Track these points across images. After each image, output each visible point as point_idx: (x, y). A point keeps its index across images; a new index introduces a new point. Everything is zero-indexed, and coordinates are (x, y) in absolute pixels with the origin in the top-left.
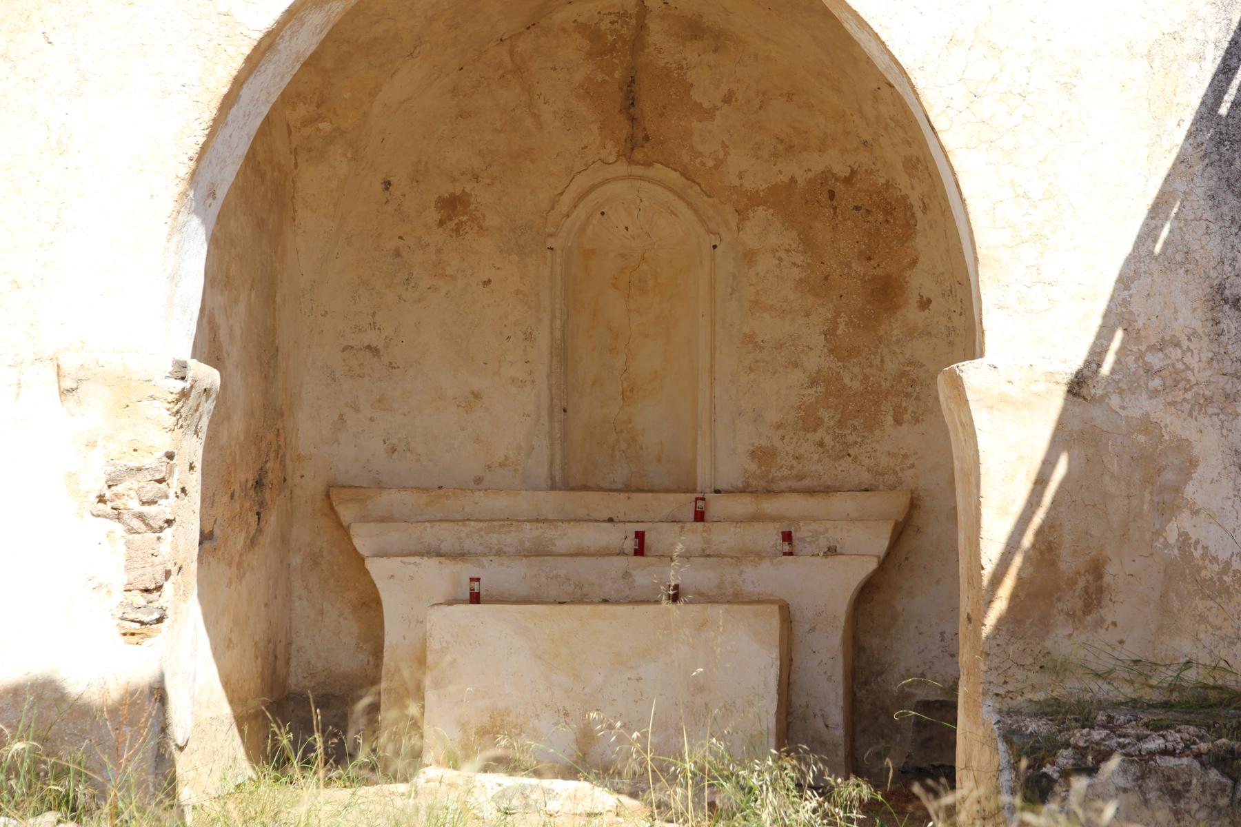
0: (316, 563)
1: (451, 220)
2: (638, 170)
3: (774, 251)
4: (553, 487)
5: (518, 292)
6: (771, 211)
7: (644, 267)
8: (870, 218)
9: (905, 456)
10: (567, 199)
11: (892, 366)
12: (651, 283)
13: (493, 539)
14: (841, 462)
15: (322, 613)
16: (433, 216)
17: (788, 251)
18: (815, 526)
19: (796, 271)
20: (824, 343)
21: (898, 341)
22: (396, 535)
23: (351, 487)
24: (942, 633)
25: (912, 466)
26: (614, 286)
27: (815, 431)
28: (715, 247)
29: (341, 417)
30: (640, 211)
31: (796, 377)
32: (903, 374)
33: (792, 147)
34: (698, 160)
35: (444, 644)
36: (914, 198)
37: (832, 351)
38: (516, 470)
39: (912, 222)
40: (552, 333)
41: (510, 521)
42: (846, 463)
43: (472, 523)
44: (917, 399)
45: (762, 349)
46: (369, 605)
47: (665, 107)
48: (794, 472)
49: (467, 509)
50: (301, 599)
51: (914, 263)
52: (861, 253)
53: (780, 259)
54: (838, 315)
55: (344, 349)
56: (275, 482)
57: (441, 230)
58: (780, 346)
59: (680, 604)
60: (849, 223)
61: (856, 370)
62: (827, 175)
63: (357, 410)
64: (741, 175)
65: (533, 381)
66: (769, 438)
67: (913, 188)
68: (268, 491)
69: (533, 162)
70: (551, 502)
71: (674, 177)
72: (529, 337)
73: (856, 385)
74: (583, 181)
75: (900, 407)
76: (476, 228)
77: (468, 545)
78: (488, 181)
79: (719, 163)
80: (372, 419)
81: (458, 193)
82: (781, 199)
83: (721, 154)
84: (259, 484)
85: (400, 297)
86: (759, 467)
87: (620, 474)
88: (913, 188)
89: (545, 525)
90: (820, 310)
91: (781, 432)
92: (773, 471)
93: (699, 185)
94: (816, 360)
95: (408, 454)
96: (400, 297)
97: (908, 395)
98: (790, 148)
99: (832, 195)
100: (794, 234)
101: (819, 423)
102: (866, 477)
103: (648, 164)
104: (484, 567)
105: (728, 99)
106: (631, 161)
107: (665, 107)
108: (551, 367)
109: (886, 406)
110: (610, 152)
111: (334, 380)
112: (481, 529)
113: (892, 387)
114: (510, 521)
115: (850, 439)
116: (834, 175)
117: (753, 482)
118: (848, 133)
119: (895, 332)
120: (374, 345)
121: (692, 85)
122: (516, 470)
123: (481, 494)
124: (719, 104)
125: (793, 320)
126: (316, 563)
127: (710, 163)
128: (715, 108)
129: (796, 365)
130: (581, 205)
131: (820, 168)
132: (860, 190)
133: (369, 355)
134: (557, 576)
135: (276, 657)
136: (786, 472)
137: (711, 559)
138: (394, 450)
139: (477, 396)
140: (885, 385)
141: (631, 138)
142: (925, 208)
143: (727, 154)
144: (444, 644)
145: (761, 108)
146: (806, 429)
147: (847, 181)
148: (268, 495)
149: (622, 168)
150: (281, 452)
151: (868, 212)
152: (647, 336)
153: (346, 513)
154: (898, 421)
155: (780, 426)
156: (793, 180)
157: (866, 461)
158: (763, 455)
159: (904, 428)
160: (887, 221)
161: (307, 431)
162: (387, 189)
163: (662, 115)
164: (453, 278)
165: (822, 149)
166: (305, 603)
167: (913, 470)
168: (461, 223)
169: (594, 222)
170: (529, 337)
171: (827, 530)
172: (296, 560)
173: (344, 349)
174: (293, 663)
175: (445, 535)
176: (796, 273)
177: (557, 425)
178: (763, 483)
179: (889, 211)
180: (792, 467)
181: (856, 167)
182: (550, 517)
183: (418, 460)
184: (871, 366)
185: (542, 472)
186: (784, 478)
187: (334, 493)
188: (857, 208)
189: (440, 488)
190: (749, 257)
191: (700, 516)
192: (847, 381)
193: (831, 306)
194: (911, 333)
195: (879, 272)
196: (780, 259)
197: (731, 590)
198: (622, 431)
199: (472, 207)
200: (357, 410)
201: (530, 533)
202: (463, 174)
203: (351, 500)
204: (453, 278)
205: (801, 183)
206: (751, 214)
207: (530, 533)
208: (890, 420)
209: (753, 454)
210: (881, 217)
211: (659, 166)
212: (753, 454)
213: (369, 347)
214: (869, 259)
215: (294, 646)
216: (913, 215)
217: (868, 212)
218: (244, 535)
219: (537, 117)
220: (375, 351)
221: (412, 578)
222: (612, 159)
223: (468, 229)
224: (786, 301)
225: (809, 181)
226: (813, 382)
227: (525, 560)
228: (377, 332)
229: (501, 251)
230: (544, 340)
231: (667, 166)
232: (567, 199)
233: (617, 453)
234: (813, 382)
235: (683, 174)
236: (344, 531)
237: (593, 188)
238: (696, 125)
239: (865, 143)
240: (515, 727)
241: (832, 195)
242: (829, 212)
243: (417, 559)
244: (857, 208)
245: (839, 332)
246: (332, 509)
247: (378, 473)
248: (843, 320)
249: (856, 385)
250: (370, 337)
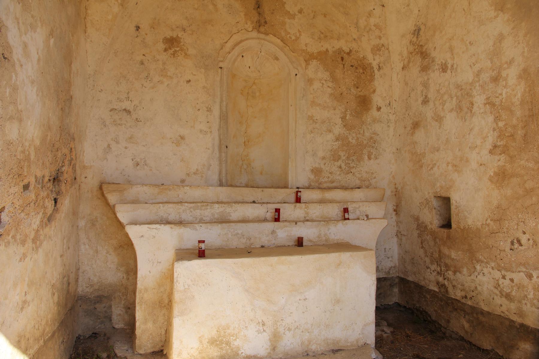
0: (93, 225)
1: (171, 49)
2: (262, 36)
3: (320, 80)
4: (221, 185)
5: (204, 87)
6: (319, 62)
7: (254, 87)
8: (357, 71)
9: (372, 173)
10: (229, 45)
11: (367, 134)
12: (257, 94)
13: (198, 213)
14: (348, 175)
15: (97, 252)
16: (161, 46)
17: (326, 81)
18: (354, 205)
19: (329, 90)
20: (341, 122)
21: (370, 123)
22: (142, 212)
23: (113, 183)
24: (385, 249)
25: (375, 178)
26: (242, 94)
27: (338, 161)
28: (296, 75)
29: (109, 146)
30: (259, 57)
31: (330, 136)
32: (371, 138)
33: (327, 36)
34: (288, 36)
35: (186, 287)
36: (375, 64)
37: (345, 126)
38: (202, 176)
39: (373, 74)
40: (221, 109)
41: (205, 203)
42: (350, 176)
43: (186, 204)
44: (376, 149)
45: (316, 123)
46: (127, 248)
47: (274, 10)
48: (330, 179)
49: (180, 196)
50: (84, 244)
51: (374, 91)
52: (354, 85)
53: (323, 84)
54: (346, 111)
55: (111, 110)
56: (69, 179)
57: (165, 53)
58: (323, 122)
60: (349, 72)
61: (354, 135)
62: (340, 51)
63: (118, 143)
64: (306, 45)
65: (211, 132)
66: (319, 164)
67: (374, 60)
68: (64, 184)
69: (213, 25)
70: (224, 193)
71: (279, 41)
72: (209, 110)
73: (354, 141)
74: (236, 38)
75: (370, 152)
76: (183, 54)
77: (184, 217)
78: (190, 32)
79: (297, 39)
80: (126, 148)
81: (175, 36)
82: (322, 57)
83: (298, 34)
84: (56, 180)
85: (142, 85)
86: (315, 177)
87: (244, 179)
88: (374, 60)
89: (226, 205)
90: (340, 108)
91: (324, 161)
92: (321, 178)
94: (338, 130)
95: (146, 167)
96: (142, 85)
97: (373, 147)
98: (326, 37)
99: (342, 59)
100: (328, 74)
101: (339, 158)
102: (358, 182)
103: (267, 34)
104: (196, 230)
105: (300, 11)
106: (259, 32)
107: (274, 10)
108: (220, 125)
109: (365, 151)
110: (249, 26)
111: (105, 126)
112: (191, 208)
113: (367, 143)
114: (205, 203)
115: (352, 165)
116: (343, 51)
117: (313, 184)
118: (348, 34)
119: (369, 120)
120: (128, 108)
121: (285, 3)
122: (202, 176)
123: (188, 188)
124: (297, 13)
125: (328, 111)
126: (93, 225)
127: (293, 38)
128: (295, 15)
129: (330, 131)
130: (237, 48)
131: (337, 47)
132: (353, 59)
133: (125, 114)
134: (237, 234)
135: (69, 284)
136: (326, 180)
137: (315, 223)
138: (138, 164)
139: (182, 138)
140: (365, 142)
141: (259, 21)
142: (380, 68)
143: (300, 35)
144: (186, 287)
145: (314, 18)
146: (334, 160)
147: (348, 54)
148: (63, 187)
149: (254, 34)
150: (73, 162)
151: (356, 68)
152: (255, 117)
153: (112, 198)
154: (370, 158)
155: (324, 158)
156: (327, 50)
157: (358, 175)
158: (317, 171)
159: (372, 161)
160: (364, 73)
161: (90, 152)
162: (138, 30)
163: (272, 13)
164: (171, 78)
165: (338, 39)
166: (87, 247)
167: (375, 180)
168: (176, 51)
170: (209, 110)
171: (360, 207)
172: (82, 223)
173: (111, 110)
174: (80, 279)
175: (171, 211)
176: (329, 90)
177: (223, 154)
178: (317, 184)
179: (364, 69)
180: (329, 177)
181: (351, 49)
182: (224, 200)
183: (151, 170)
184: (360, 134)
185: (216, 177)
186: (326, 182)
187: (105, 187)
188: (352, 66)
189: (163, 184)
190: (310, 81)
191: (298, 200)
192: (350, 140)
193: (343, 106)
194: (374, 121)
195: (361, 94)
196: (323, 84)
197: (324, 238)
198: (244, 160)
199: (182, 44)
200: (118, 143)
201: (217, 209)
202: (177, 27)
203: (114, 191)
204: (171, 78)
205: (331, 53)
206: (311, 63)
207: (217, 209)
208: (366, 157)
209: (312, 171)
210: (361, 71)
211: (271, 36)
212: (312, 171)
213: (125, 110)
214: (357, 88)
215: (81, 270)
216: (374, 71)
217: (356, 68)
218: (40, 215)
219: (215, 5)
220: (128, 112)
221: (154, 237)
222: (250, 29)
223: (179, 54)
224: (326, 102)
225: (334, 52)
226: (337, 139)
227: (219, 225)
228: (130, 102)
229: (196, 67)
230: (216, 112)
231: (275, 36)
232: (229, 45)
233: (243, 170)
234: (337, 139)
235: (282, 41)
236: (112, 209)
237: (241, 41)
238: (287, 20)
239: (354, 39)
240: (233, 336)
241: (342, 59)
242: (342, 66)
243: (157, 226)
244: (352, 66)
245: (347, 118)
246: (103, 195)
247: (129, 176)
248: (348, 112)
249: (354, 141)
250: (126, 105)
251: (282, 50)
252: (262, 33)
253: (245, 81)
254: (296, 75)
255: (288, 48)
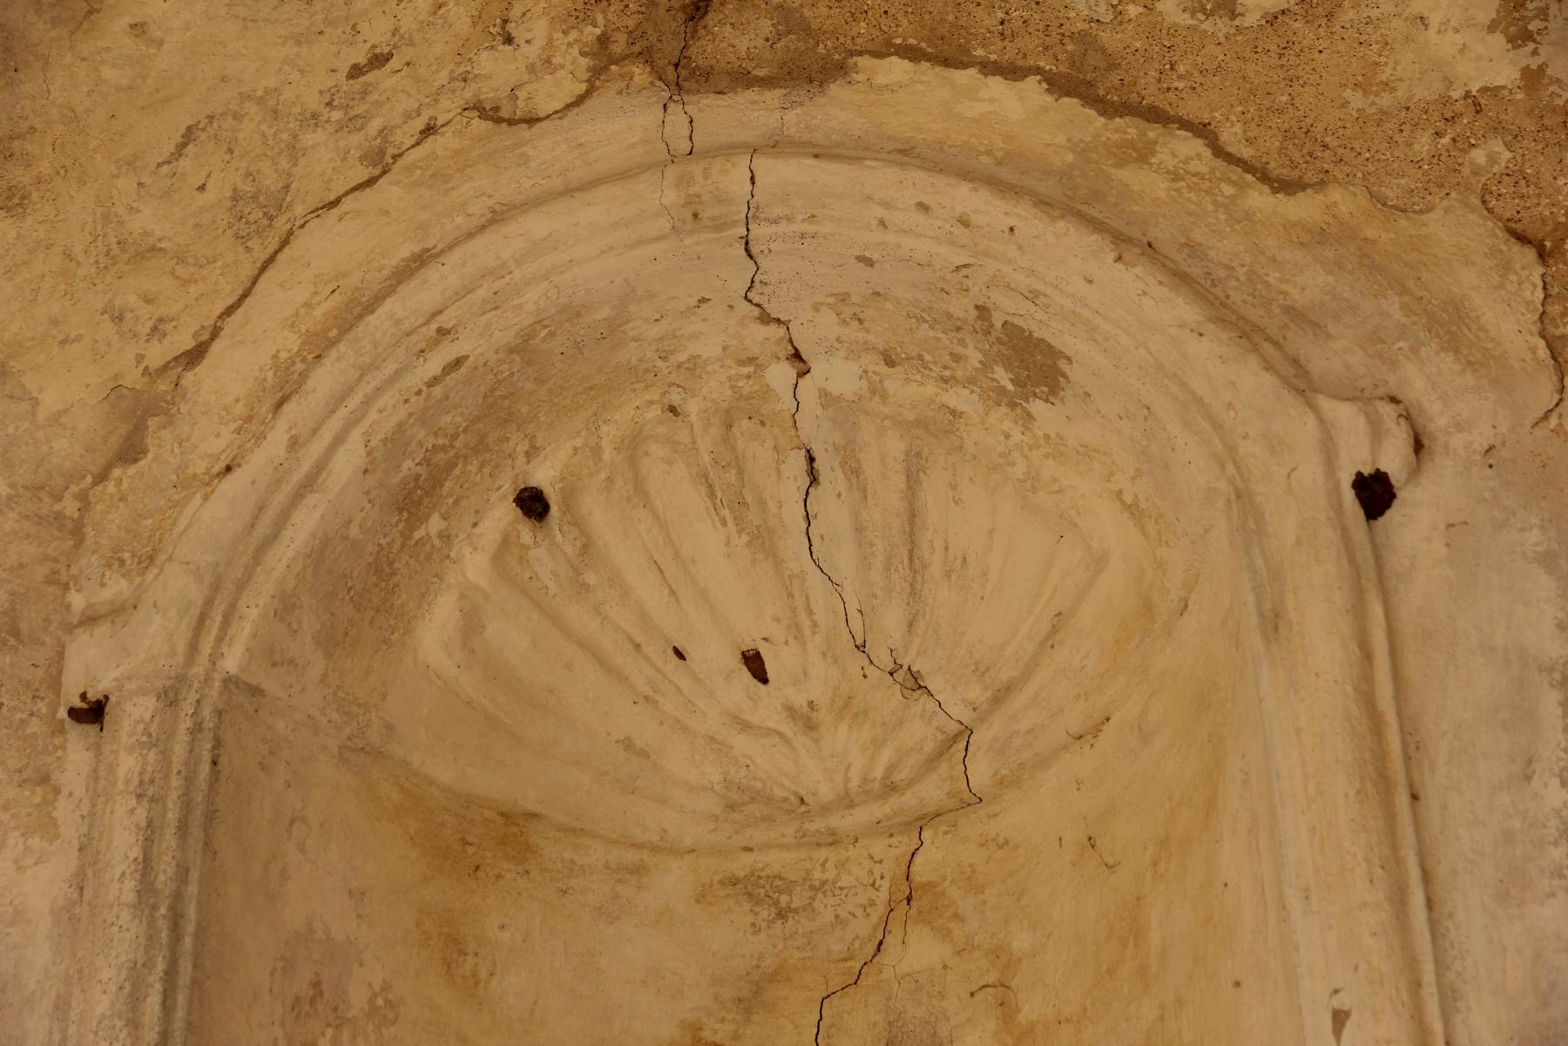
7: (918, 951)
28: (1375, 494)
59: (1406, 496)
71: (1015, 110)
93: (1202, 130)
103: (810, 68)
106: (683, 77)
149: (629, 121)
169: (473, 565)
211: (897, 68)
231: (950, 60)
235: (1058, 85)
249: (1070, 157)
251: (1074, 200)
252: (743, 79)
253: (761, 893)
254: (1375, 494)
255: (1189, 147)
